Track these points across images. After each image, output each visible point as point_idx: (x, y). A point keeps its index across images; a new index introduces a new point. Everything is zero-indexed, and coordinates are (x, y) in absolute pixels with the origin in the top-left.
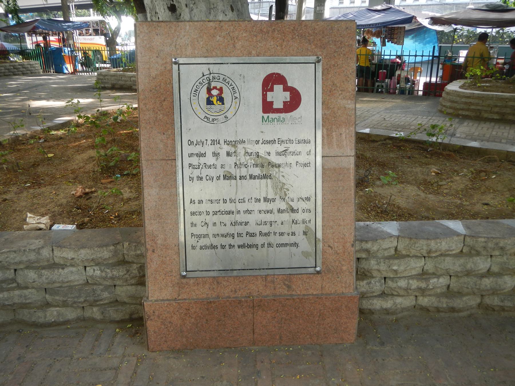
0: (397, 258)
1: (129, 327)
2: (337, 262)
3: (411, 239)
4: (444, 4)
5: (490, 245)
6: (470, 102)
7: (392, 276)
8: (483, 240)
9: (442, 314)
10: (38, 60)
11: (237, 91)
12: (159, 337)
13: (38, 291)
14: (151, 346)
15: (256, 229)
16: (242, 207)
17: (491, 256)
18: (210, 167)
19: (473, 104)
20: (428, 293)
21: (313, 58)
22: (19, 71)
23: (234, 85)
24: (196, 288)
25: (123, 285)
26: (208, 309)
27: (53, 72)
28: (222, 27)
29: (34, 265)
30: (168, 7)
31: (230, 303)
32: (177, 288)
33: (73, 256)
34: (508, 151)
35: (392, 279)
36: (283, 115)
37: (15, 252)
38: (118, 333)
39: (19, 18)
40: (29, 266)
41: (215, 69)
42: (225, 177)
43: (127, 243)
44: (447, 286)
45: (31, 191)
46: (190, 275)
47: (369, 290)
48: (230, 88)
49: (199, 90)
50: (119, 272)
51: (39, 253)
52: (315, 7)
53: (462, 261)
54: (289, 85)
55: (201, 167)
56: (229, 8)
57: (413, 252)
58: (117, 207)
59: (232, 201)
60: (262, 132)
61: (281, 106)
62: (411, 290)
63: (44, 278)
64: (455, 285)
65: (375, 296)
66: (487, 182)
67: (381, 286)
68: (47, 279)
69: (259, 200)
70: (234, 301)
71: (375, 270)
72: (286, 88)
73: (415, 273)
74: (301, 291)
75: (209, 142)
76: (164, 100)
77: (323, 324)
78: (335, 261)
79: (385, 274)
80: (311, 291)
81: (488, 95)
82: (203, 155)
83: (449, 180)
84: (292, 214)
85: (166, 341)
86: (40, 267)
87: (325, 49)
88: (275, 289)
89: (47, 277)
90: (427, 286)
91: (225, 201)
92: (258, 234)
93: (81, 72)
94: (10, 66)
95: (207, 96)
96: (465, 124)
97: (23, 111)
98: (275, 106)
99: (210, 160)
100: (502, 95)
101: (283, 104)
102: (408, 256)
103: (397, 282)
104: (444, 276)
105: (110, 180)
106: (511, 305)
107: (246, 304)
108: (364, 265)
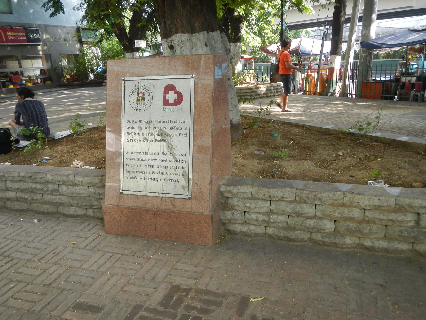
2: (200, 193)
7: (248, 211)
11: (151, 94)
12: (110, 225)
16: (150, 157)
18: (137, 134)
23: (150, 91)
24: (127, 200)
26: (132, 213)
31: (143, 211)
32: (118, 199)
33: (82, 180)
36: (174, 107)
37: (58, 175)
40: (65, 183)
42: (144, 140)
46: (124, 192)
53: (293, 205)
54: (177, 90)
55: (132, 134)
56: (205, 45)
57: (261, 196)
59: (147, 153)
60: (163, 116)
63: (69, 190)
67: (242, 216)
68: (70, 191)
70: (144, 209)
72: (176, 92)
73: (264, 211)
74: (180, 209)
75: (137, 121)
78: (199, 193)
80: (185, 209)
85: (113, 229)
88: (166, 205)
90: (269, 220)
91: (143, 153)
92: (158, 173)
98: (170, 102)
101: (173, 101)
102: (259, 199)
104: (283, 215)
106: (329, 241)
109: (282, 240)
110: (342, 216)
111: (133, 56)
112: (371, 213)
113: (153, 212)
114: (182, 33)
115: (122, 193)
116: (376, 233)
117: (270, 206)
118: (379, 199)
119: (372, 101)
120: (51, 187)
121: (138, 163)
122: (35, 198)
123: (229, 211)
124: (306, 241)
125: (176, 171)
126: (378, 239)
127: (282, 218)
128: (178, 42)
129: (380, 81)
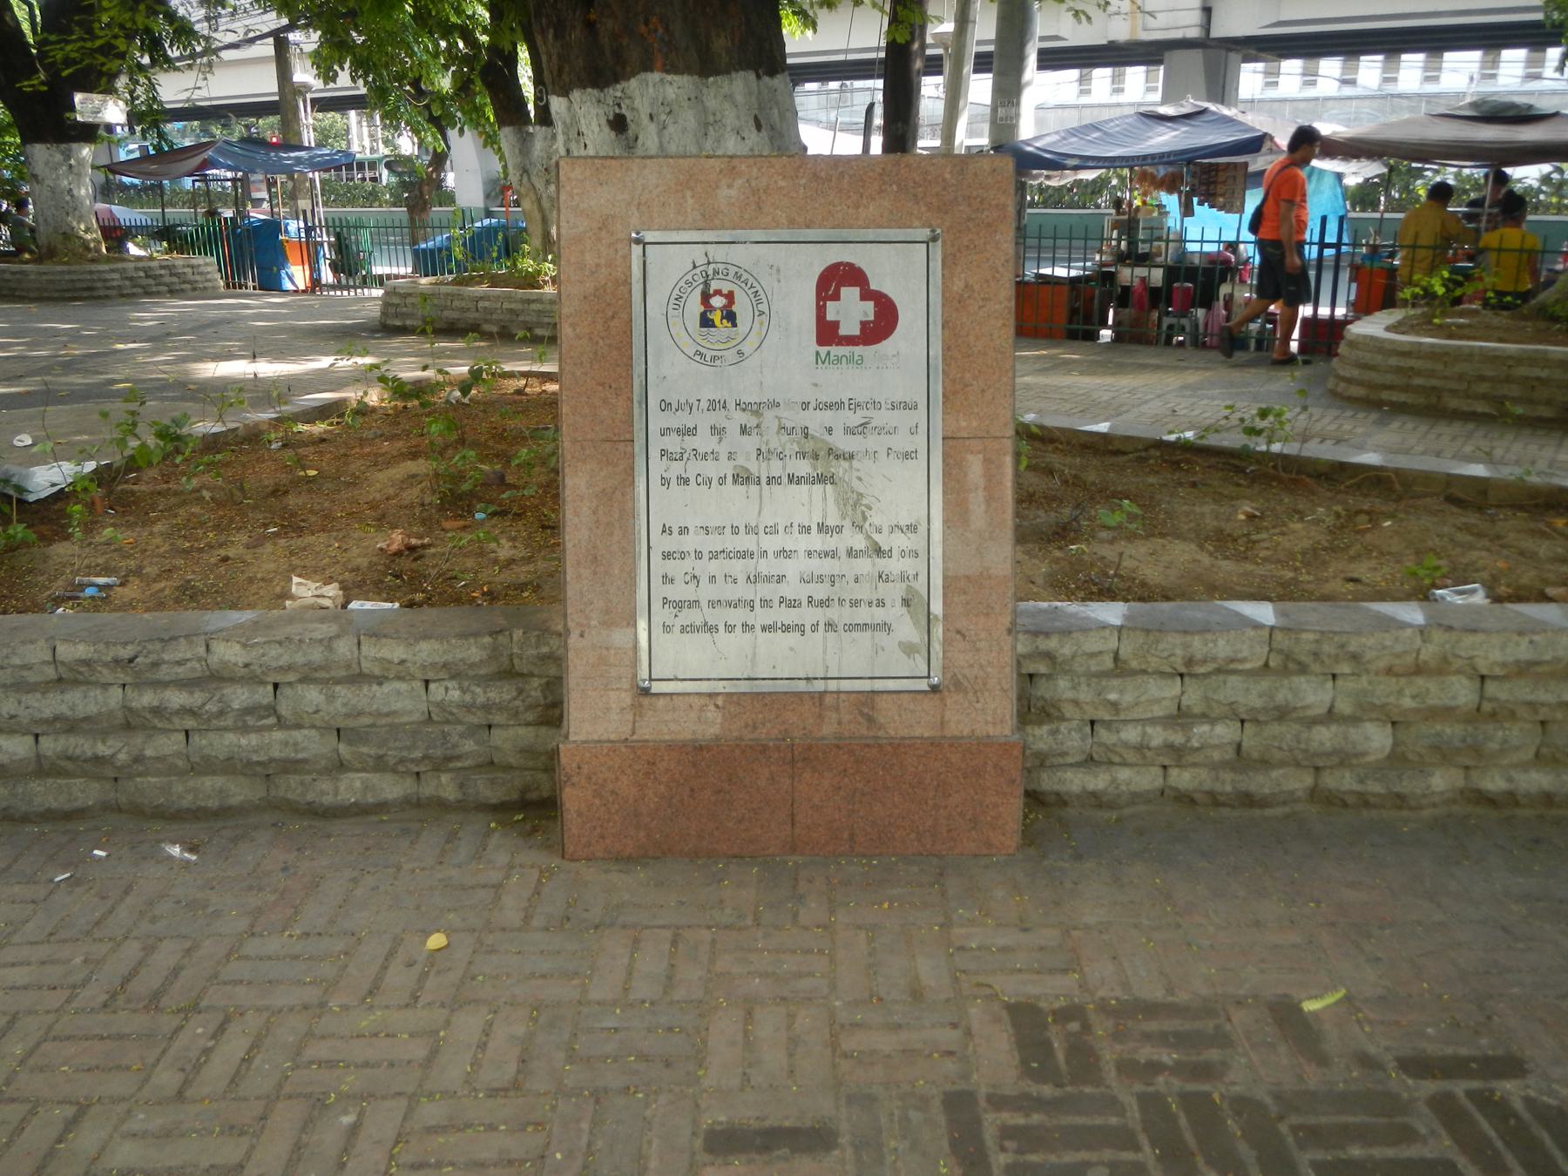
0: (1117, 676)
1: (518, 821)
3: (1148, 631)
4: (1392, 96)
5: (1327, 648)
6: (1412, 369)
7: (1107, 717)
8: (1311, 637)
9: (1225, 811)
10: (212, 255)
11: (765, 300)
13: (322, 735)
14: (570, 848)
15: (802, 592)
16: (771, 543)
17: (1334, 676)
18: (705, 457)
19: (1419, 373)
20: (1190, 759)
21: (925, 233)
22: (159, 284)
23: (758, 288)
25: (508, 726)
26: (694, 765)
27: (254, 288)
28: (734, 168)
29: (317, 675)
30: (608, 121)
31: (743, 752)
33: (404, 657)
34: (1449, 475)
35: (1108, 724)
36: (858, 350)
37: (280, 643)
38: (494, 830)
39: (161, 135)
41: (718, 253)
43: (521, 632)
44: (1234, 746)
45: (282, 542)
46: (657, 687)
47: (1055, 746)
48: (750, 292)
49: (685, 296)
50: (502, 693)
51: (330, 648)
52: (994, 109)
53: (1265, 684)
54: (873, 287)
56: (752, 122)
57: (1154, 663)
58: (484, 576)
59: (750, 530)
61: (857, 332)
62: (1149, 749)
63: (338, 703)
64: (1252, 743)
65: (1071, 765)
66: (1368, 536)
67: (1083, 740)
68: (345, 705)
69: (808, 530)
70: (751, 747)
71: (1066, 700)
72: (867, 294)
73: (1161, 714)
75: (704, 405)
76: (613, 317)
77: (946, 807)
79: (1091, 713)
81: (1460, 347)
82: (691, 432)
83: (1277, 531)
84: (878, 560)
86: (329, 679)
87: (946, 213)
89: (345, 701)
91: (735, 530)
92: (805, 602)
93: (333, 287)
94: (137, 269)
95: (702, 309)
96: (1395, 425)
97: (192, 387)
98: (843, 331)
99: (703, 442)
100: (1495, 349)
103: (1118, 732)
104: (1228, 722)
105: (462, 523)
106: (1382, 791)
107: (776, 755)
108: (1043, 690)
109: (1224, 805)
110: (1422, 706)
111: (68, 157)
112: (1507, 686)
113: (789, 755)
114: (668, 72)
115: (646, 692)
116: (1518, 748)
117: (1183, 693)
118: (1531, 642)
119: (1056, 346)
120: (239, 697)
121: (715, 567)
122: (149, 752)
123: (1040, 723)
124: (1296, 801)
125: (880, 589)
126: (1524, 766)
127: (1225, 732)
128: (652, 104)
129: (1052, 277)
